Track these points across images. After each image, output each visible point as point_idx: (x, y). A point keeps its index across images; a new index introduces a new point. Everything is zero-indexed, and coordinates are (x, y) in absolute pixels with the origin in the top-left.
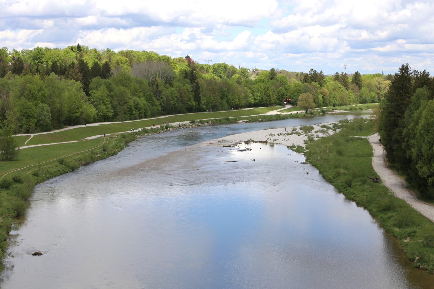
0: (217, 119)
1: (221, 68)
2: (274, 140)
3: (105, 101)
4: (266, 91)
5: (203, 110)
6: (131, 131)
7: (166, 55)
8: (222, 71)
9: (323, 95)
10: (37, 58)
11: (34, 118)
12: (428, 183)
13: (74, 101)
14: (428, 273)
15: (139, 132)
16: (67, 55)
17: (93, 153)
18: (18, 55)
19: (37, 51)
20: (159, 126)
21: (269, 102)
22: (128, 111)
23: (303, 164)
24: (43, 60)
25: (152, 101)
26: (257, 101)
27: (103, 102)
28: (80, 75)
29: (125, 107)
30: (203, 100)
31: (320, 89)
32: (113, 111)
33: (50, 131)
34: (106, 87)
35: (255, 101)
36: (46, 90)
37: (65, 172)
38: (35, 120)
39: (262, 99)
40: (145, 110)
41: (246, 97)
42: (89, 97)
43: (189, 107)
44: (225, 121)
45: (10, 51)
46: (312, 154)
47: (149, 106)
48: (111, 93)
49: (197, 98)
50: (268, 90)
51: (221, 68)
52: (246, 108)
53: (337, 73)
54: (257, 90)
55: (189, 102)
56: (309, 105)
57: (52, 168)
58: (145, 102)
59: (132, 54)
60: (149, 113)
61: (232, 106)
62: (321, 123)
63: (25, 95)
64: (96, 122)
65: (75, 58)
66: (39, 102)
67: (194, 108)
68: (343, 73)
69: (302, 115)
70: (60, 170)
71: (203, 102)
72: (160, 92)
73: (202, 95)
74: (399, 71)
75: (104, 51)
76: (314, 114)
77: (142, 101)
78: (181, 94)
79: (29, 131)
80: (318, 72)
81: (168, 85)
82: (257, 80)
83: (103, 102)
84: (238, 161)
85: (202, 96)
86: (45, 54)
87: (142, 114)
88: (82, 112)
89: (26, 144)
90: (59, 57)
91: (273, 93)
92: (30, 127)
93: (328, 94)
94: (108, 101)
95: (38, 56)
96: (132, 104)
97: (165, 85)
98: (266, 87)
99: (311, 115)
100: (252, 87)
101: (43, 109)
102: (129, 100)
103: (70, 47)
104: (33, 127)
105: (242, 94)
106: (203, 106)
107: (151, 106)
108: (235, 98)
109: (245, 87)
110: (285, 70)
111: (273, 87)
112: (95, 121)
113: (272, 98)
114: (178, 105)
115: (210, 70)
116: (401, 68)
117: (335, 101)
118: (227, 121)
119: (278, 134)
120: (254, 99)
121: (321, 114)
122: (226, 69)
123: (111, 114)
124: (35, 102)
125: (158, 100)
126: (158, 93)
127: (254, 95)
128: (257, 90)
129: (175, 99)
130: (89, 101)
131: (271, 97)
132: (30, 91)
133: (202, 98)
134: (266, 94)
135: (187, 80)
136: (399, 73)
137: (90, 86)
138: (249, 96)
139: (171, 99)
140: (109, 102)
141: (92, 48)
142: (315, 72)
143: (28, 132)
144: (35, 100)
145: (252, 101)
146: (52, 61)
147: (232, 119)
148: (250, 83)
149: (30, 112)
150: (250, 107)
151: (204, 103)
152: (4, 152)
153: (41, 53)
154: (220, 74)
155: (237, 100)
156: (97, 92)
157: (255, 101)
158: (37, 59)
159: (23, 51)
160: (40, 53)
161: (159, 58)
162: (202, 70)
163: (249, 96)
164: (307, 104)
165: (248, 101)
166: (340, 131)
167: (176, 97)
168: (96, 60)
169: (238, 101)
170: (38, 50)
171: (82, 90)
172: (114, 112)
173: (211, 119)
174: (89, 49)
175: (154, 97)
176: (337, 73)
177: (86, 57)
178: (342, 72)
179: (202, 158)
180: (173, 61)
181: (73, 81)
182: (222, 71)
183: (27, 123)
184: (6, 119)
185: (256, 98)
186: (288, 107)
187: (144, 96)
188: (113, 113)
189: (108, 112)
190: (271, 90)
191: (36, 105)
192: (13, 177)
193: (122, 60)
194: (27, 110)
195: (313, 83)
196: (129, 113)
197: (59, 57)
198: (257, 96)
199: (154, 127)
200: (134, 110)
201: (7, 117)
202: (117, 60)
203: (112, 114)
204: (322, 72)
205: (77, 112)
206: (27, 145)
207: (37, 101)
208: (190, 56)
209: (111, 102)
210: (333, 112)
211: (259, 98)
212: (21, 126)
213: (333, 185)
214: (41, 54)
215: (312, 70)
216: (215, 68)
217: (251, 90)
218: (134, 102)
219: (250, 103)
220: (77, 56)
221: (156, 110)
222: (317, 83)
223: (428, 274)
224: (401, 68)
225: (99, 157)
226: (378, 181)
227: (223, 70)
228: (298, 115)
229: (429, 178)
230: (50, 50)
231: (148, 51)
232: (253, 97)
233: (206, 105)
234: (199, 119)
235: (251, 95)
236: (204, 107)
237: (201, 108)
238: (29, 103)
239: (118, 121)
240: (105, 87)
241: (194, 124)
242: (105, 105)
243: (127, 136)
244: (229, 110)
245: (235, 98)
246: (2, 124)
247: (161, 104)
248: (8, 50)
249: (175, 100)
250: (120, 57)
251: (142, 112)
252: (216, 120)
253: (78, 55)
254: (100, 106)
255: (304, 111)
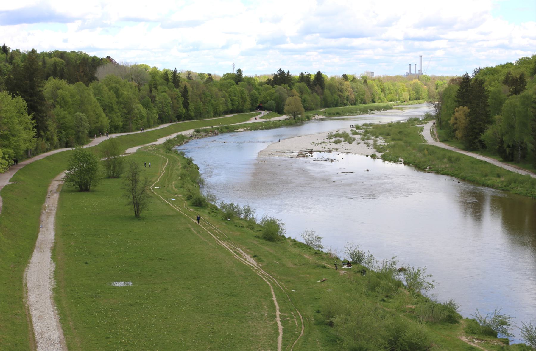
30: (191, 107)
49: (186, 105)
67: (183, 116)
68: (307, 74)
80: (286, 72)
84: (354, 172)
132: (63, 98)
142: (283, 72)
169: (340, 103)
184: (49, 131)
215: (280, 70)
231: (77, 51)
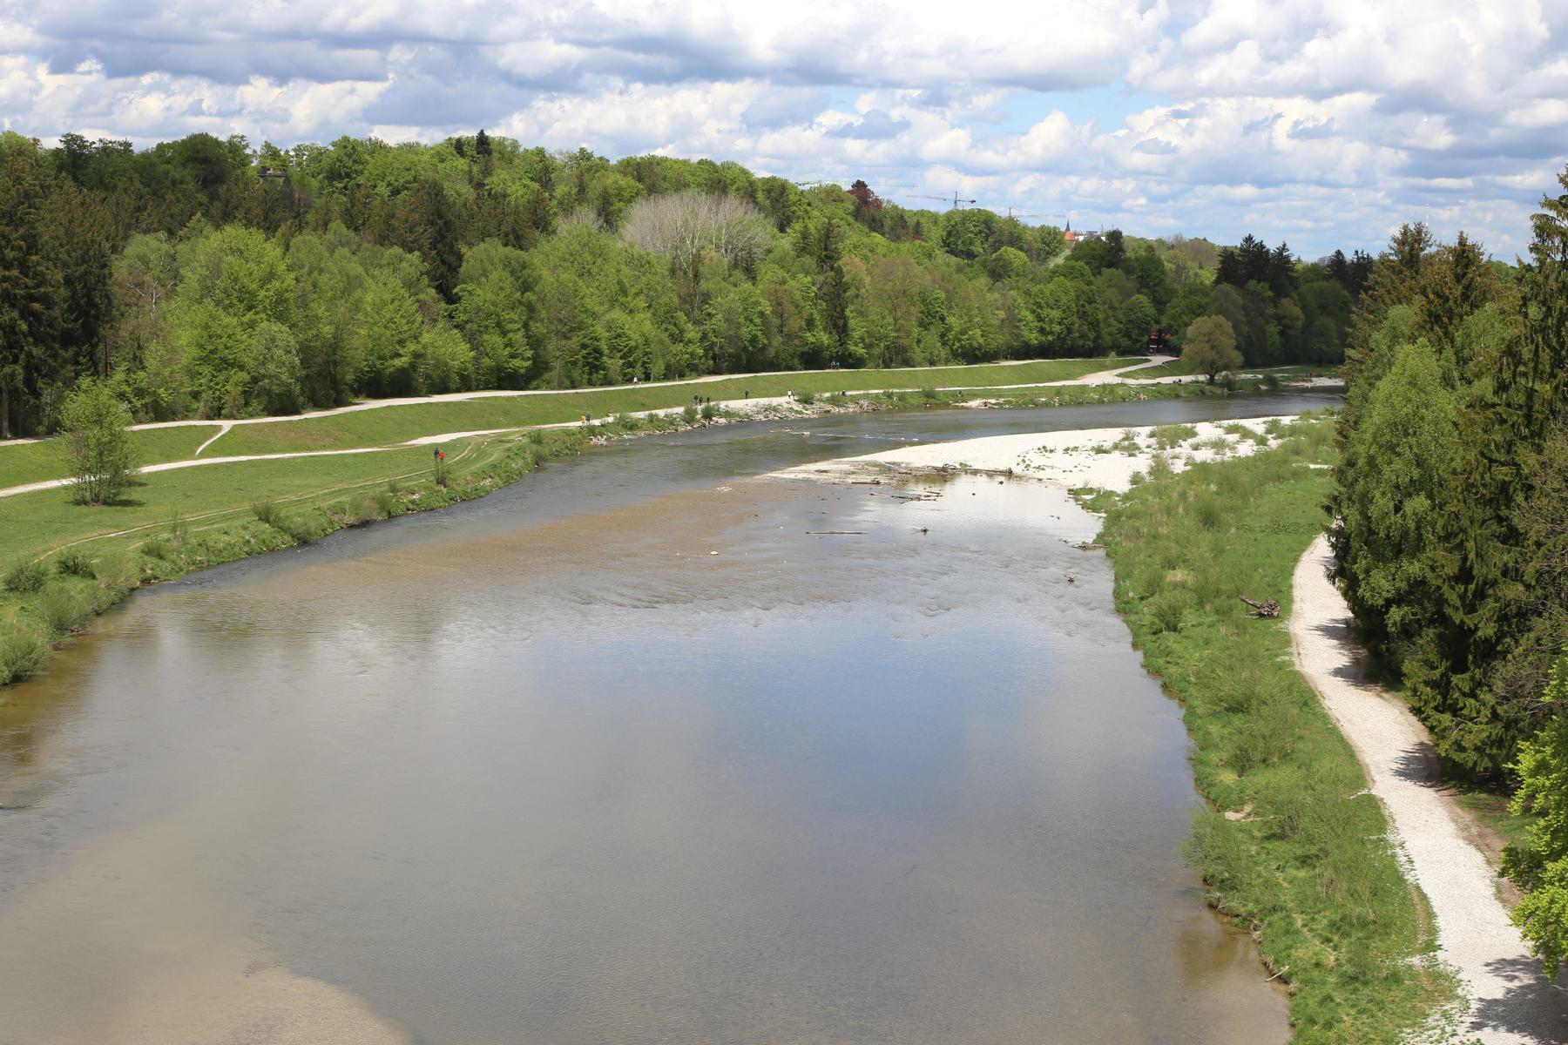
0: (892, 393)
1: (975, 226)
2: (1039, 468)
3: (504, 320)
4: (1083, 306)
5: (856, 363)
6: (579, 424)
7: (778, 176)
8: (976, 235)
9: (1287, 327)
10: (340, 174)
11: (242, 368)
12: (1387, 625)
13: (392, 318)
14: (1236, 926)
15: (602, 426)
16: (441, 166)
17: (394, 489)
18: (279, 163)
19: (342, 153)
20: (680, 410)
21: (1093, 342)
22: (584, 357)
23: (1080, 551)
24: (361, 180)
25: (675, 325)
26: (1050, 338)
27: (499, 325)
28: (426, 235)
29: (575, 341)
30: (857, 327)
31: (1276, 307)
32: (529, 354)
33: (298, 413)
34: (513, 273)
35: (1043, 338)
36: (290, 279)
37: (267, 546)
38: (244, 376)
39: (1069, 331)
40: (646, 354)
41: (1012, 321)
42: (453, 306)
43: (806, 349)
44: (922, 400)
45: (255, 146)
46: (1123, 518)
47: (661, 342)
48: (525, 295)
49: (840, 327)
50: (1090, 302)
51: (975, 226)
52: (1011, 359)
53: (1339, 253)
54: (1052, 301)
55: (808, 334)
56: (1221, 357)
57: (226, 533)
58: (648, 327)
59: (658, 169)
60: (658, 367)
61: (960, 351)
62: (1264, 413)
63: (217, 291)
64: (469, 389)
65: (467, 177)
66: (263, 316)
69: (1192, 389)
70: (252, 539)
71: (856, 335)
72: (706, 297)
73: (855, 311)
74: (1391, 248)
75: (571, 158)
76: (1237, 386)
77: (639, 326)
78: (780, 304)
79: (223, 412)
80: (1272, 246)
81: (738, 274)
82: (1059, 266)
83: (499, 325)
85: (854, 314)
86: (367, 163)
87: (633, 367)
88: (416, 355)
89: (200, 453)
90: (413, 172)
91: (1110, 313)
92: (227, 397)
93: (1300, 323)
94: (516, 322)
95: (344, 166)
96: (600, 330)
97: (730, 276)
98: (1083, 292)
99: (1226, 390)
100: (1035, 289)
101: (273, 340)
102: (590, 321)
103: (454, 142)
104: (234, 399)
105: (997, 312)
106: (854, 348)
107: (667, 340)
108: (969, 324)
109: (1012, 289)
110: (1205, 240)
111: (1112, 295)
112: (466, 386)
113: (1104, 331)
114: (766, 342)
115: (936, 234)
116: (1398, 235)
117: (1324, 348)
118: (925, 399)
119: (1066, 450)
120: (1042, 331)
121: (1263, 387)
122: (989, 229)
123: (521, 365)
124: (250, 316)
125: (696, 323)
126: (696, 302)
127: (1040, 319)
128: (1052, 301)
129: (758, 321)
130: (453, 317)
131: (1101, 325)
133: (852, 323)
134: (1083, 315)
135: (809, 261)
136: (1390, 254)
137: (462, 270)
138: (1020, 321)
139: (742, 320)
140: (517, 326)
141: (531, 147)
143: (217, 413)
144: (250, 308)
145: (1033, 338)
146: (389, 184)
147: (945, 393)
148: (1031, 276)
149: (228, 348)
150: (1027, 356)
151: (862, 339)
152: (93, 479)
153: (354, 156)
154: (971, 244)
155: (978, 332)
156: (479, 291)
157: (1043, 338)
158: (340, 177)
159: (298, 150)
160: (350, 156)
161: (751, 184)
162: (900, 231)
163: (1020, 321)
164: (1214, 352)
165: (1018, 336)
166: (1281, 446)
167: (762, 314)
168: (536, 186)
170: (345, 147)
171: (425, 280)
172: (535, 358)
173: (870, 392)
174: (521, 150)
175: (680, 314)
176: (1339, 253)
177: (502, 176)
178: (1357, 252)
179: (756, 519)
180: (797, 198)
181: (397, 250)
182: (976, 235)
183: (217, 384)
184: (143, 368)
185: (1048, 329)
186: (1158, 360)
187: (649, 307)
188: (530, 362)
189: (513, 356)
190: (1104, 303)
191: (252, 325)
192: (63, 559)
193: (620, 189)
194: (219, 341)
195: (1252, 284)
196: (588, 364)
197: (413, 172)
198: (1052, 323)
199: (661, 413)
200: (606, 352)
201: (146, 364)
202: (605, 188)
203: (528, 364)
204: (1284, 249)
205: (401, 352)
206: (202, 455)
207: (257, 313)
208: (866, 183)
209: (526, 325)
210: (1306, 384)
211: (1057, 328)
212: (196, 395)
213: (1127, 622)
214: (355, 162)
216: (953, 226)
217: (1032, 301)
218: (609, 329)
219: (1027, 345)
220: (471, 171)
221: (687, 356)
222: (1266, 285)
223: (1234, 929)
224: (1398, 235)
225: (413, 502)
226: (1275, 614)
227: (980, 232)
228: (1180, 388)
229: (1394, 609)
230: (385, 147)
232: (1036, 324)
233: (868, 347)
234: (827, 391)
235: (1030, 317)
236: (860, 350)
237: (850, 354)
238: (227, 320)
239: (547, 389)
240: (505, 274)
241: (808, 406)
242: (504, 333)
243: (556, 438)
244: (946, 365)
245: (969, 324)
246: (129, 385)
247: (704, 337)
248: (247, 145)
249: (756, 326)
250: (619, 177)
251: (635, 361)
252: (890, 396)
253: (475, 169)
254: (486, 337)
255: (1202, 378)
